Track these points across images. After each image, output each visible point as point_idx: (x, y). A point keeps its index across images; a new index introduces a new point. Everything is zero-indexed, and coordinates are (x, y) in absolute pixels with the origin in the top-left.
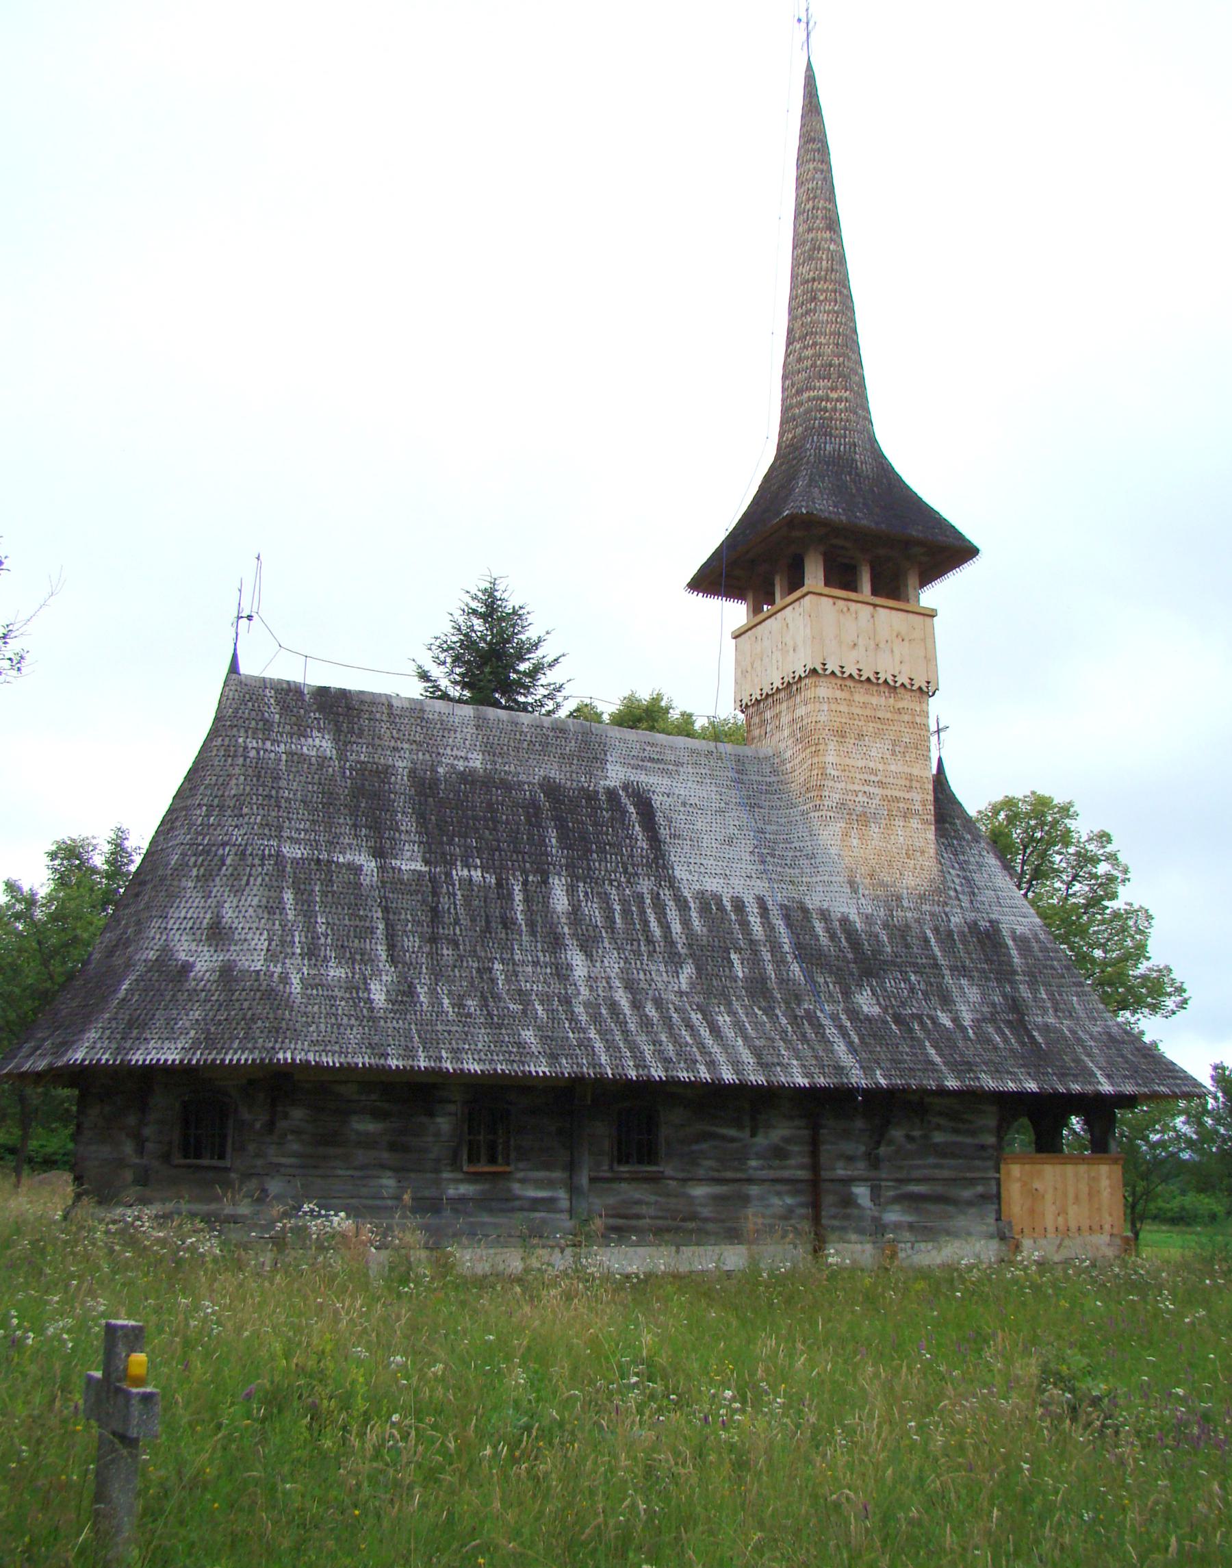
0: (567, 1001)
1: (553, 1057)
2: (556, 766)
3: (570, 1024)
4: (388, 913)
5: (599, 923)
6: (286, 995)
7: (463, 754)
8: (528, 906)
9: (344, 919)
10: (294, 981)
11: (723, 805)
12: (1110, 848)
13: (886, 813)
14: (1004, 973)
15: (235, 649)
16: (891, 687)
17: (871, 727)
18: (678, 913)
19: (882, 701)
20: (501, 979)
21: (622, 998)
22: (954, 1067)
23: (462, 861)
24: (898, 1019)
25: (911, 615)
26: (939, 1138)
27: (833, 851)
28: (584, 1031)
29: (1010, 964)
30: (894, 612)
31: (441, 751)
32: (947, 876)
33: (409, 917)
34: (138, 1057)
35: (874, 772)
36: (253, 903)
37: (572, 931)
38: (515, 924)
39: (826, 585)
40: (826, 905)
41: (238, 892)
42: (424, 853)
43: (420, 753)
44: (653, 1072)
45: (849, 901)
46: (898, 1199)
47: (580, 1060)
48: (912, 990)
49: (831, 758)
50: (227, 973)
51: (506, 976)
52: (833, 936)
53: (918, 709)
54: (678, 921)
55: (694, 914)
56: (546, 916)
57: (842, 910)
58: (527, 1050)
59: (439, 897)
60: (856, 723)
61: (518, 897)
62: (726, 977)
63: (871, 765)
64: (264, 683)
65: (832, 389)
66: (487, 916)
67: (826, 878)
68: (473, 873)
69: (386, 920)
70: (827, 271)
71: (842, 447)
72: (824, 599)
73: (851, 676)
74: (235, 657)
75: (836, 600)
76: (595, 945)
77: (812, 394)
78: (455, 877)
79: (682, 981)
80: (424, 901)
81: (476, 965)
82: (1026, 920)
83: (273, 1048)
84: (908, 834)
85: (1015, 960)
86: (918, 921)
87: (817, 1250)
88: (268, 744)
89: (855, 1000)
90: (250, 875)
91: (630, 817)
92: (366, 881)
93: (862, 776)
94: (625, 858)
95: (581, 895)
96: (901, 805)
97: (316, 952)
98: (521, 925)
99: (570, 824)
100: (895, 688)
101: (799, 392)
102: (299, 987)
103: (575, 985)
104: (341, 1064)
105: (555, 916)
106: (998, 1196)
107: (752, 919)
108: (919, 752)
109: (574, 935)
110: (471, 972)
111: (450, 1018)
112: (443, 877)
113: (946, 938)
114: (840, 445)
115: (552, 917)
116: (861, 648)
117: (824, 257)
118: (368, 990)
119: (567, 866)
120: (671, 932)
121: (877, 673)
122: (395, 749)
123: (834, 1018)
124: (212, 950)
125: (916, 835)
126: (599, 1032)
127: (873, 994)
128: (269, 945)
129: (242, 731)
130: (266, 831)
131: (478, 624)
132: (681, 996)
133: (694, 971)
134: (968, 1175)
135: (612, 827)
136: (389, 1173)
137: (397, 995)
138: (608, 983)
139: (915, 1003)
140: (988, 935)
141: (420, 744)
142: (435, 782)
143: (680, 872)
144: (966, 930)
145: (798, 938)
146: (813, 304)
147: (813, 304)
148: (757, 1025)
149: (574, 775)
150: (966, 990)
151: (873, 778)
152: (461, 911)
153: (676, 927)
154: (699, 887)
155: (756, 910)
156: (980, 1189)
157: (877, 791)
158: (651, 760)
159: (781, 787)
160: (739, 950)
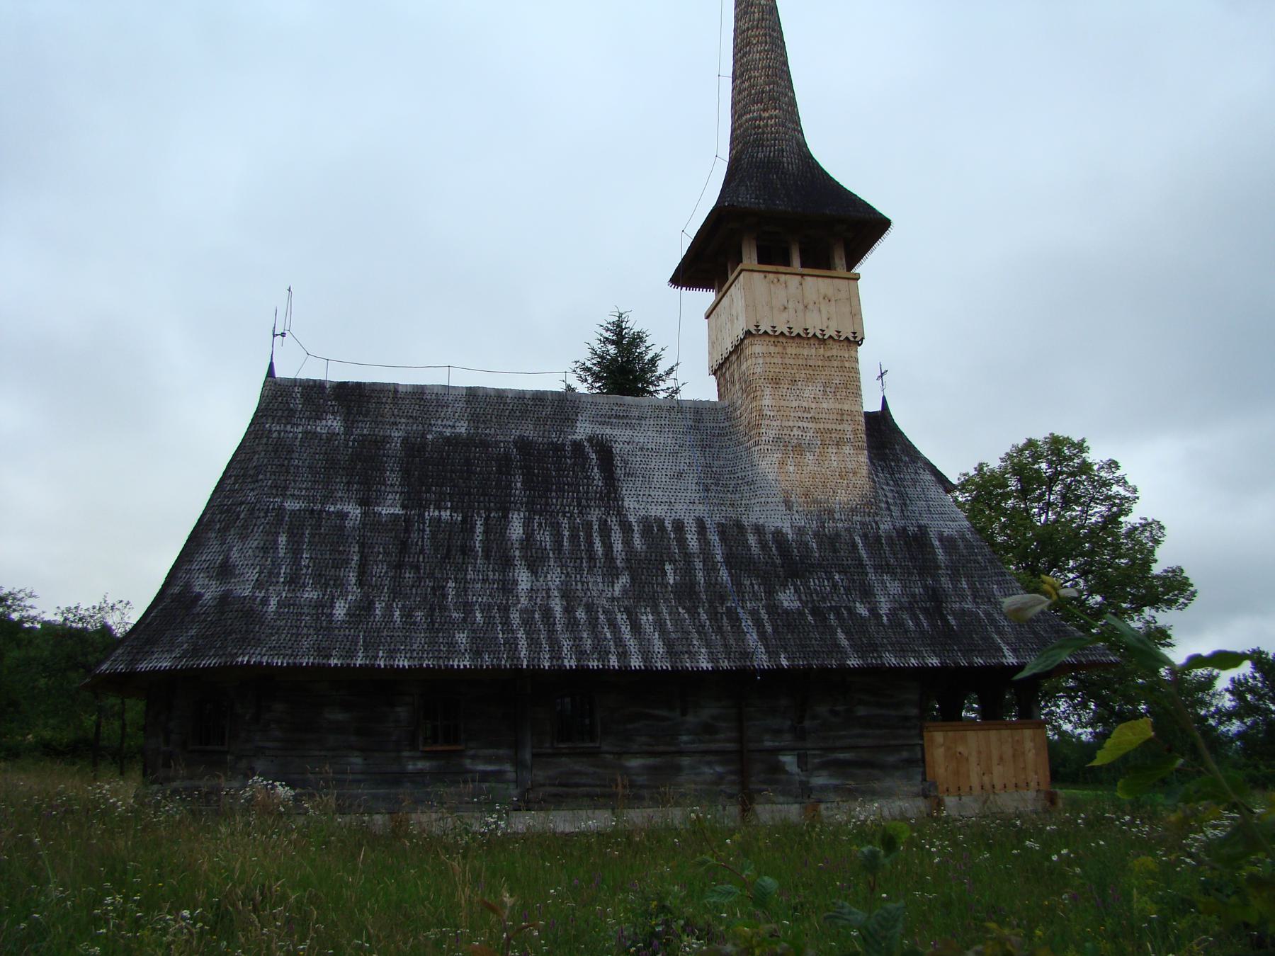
0: (505, 610)
1: (477, 653)
2: (531, 427)
3: (502, 627)
4: (364, 548)
5: (548, 547)
6: (262, 613)
7: (451, 424)
8: (487, 536)
9: (326, 554)
10: (272, 603)
11: (677, 447)
12: (1118, 473)
13: (819, 443)
14: (926, 566)
15: (272, 359)
16: (822, 340)
17: (803, 374)
18: (621, 535)
20: (451, 593)
21: (557, 606)
22: (860, 650)
23: (435, 505)
24: (814, 612)
26: (861, 711)
27: (771, 477)
28: (513, 631)
29: (935, 560)
30: (820, 279)
31: (433, 422)
32: (880, 492)
33: (381, 550)
34: (143, 666)
35: (806, 410)
36: (253, 546)
37: (522, 554)
38: (473, 551)
39: (759, 263)
40: (761, 521)
41: (243, 538)
42: (404, 500)
43: (415, 425)
44: (566, 663)
45: (783, 517)
46: (825, 766)
47: (501, 655)
48: (835, 586)
49: (767, 401)
50: (224, 600)
51: (457, 591)
52: (764, 546)
53: (846, 356)
54: (620, 542)
55: (636, 535)
56: (501, 543)
57: (776, 525)
58: (457, 648)
59: (410, 533)
60: (789, 371)
61: (479, 529)
62: (657, 584)
63: (805, 404)
64: (295, 382)
65: (765, 110)
66: (449, 546)
67: (763, 500)
68: (443, 513)
69: (362, 553)
70: (759, 20)
71: (772, 154)
72: (756, 274)
73: (782, 333)
74: (271, 365)
75: (767, 274)
76: (542, 564)
77: (748, 116)
78: (427, 517)
79: (616, 588)
80: (396, 537)
81: (431, 584)
82: (954, 523)
83: (236, 654)
84: (841, 459)
87: (746, 809)
88: (289, 427)
89: (776, 598)
90: (255, 525)
92: (349, 524)
93: (796, 414)
94: (581, 495)
95: (536, 525)
96: (833, 435)
97: (297, 580)
98: (478, 551)
99: (536, 471)
100: (825, 340)
101: (740, 117)
102: (275, 607)
103: (517, 596)
104: (288, 664)
105: (509, 543)
106: (923, 760)
107: (689, 537)
109: (522, 558)
110: (426, 590)
111: (396, 626)
112: (416, 517)
113: (873, 541)
114: (770, 152)
115: (506, 544)
116: (791, 311)
117: (756, 10)
118: (332, 607)
119: (527, 503)
120: (613, 551)
121: (807, 329)
122: (395, 424)
123: (754, 614)
124: (218, 583)
126: (527, 633)
127: (796, 591)
128: (259, 576)
129: (270, 419)
130: (274, 492)
131: (612, 349)
132: (613, 601)
133: (628, 581)
134: (892, 742)
135: (573, 471)
136: (356, 753)
137: (356, 610)
138: (547, 593)
139: (835, 598)
140: (915, 537)
141: (416, 418)
142: (424, 446)
143: (629, 503)
144: (895, 534)
145: (731, 549)
146: (748, 48)
147: (748, 48)
148: (677, 621)
149: (546, 433)
150: (888, 585)
151: (806, 415)
152: (427, 542)
153: (618, 546)
154: (644, 513)
155: (693, 529)
156: (905, 755)
157: (810, 425)
158: (617, 417)
159: (732, 430)
160: (673, 561)
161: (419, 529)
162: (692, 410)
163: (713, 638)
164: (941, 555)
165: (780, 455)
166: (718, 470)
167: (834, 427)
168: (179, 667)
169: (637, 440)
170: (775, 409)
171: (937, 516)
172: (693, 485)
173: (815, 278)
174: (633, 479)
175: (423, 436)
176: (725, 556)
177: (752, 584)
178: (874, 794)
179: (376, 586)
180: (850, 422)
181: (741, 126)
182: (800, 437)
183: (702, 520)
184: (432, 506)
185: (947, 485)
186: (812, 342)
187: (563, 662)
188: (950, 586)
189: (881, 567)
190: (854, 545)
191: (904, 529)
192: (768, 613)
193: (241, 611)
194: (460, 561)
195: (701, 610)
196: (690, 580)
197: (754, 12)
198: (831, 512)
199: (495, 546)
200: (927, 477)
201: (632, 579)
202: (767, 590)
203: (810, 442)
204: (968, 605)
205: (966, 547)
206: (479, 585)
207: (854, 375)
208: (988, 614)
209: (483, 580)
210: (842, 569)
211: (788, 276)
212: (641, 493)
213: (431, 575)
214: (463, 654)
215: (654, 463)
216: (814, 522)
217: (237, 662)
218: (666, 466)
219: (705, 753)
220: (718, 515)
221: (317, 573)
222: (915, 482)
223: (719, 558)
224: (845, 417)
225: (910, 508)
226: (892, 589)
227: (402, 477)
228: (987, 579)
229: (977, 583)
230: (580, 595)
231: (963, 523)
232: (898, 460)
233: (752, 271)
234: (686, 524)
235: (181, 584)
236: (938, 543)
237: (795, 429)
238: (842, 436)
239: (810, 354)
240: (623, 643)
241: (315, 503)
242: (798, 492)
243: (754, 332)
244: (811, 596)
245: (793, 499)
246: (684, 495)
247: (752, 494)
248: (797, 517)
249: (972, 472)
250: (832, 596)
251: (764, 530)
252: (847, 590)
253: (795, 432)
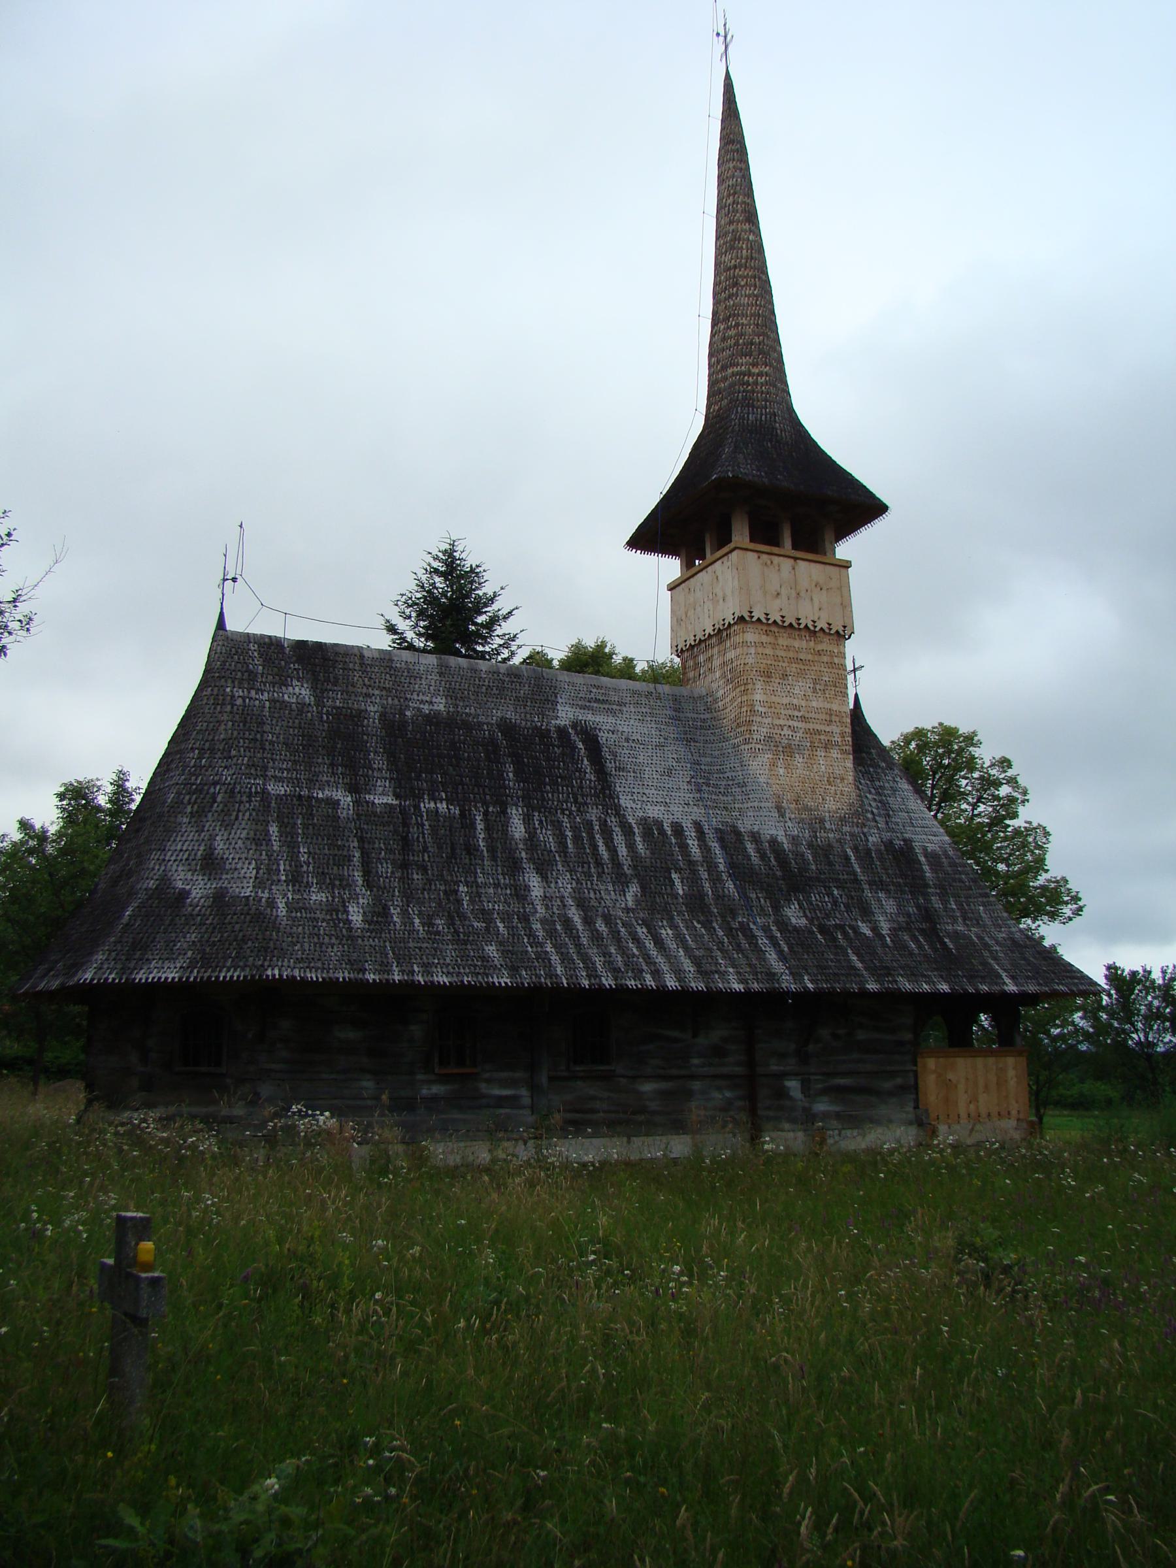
0: (525, 919)
1: (514, 970)
3: (529, 939)
4: (363, 842)
6: (273, 918)
7: (428, 699)
10: (280, 905)
12: (1010, 773)
13: (808, 744)
14: (917, 886)
15: (222, 608)
16: (812, 632)
19: (804, 644)
23: (429, 795)
24: (823, 930)
25: (828, 567)
26: (861, 1035)
27: (762, 779)
29: (923, 878)
30: (813, 565)
31: (409, 696)
34: (141, 976)
35: (797, 708)
36: (242, 836)
37: (529, 856)
38: (478, 850)
40: (756, 828)
41: (228, 826)
42: (395, 788)
43: (390, 699)
46: (826, 1091)
48: (835, 903)
49: (758, 696)
50: (220, 899)
51: (470, 897)
52: (763, 856)
53: (836, 651)
54: (624, 845)
56: (506, 843)
57: (771, 832)
59: (409, 828)
62: (667, 894)
63: (795, 701)
64: (248, 638)
65: (754, 365)
66: (452, 844)
67: (756, 804)
69: (362, 848)
70: (747, 258)
71: (763, 417)
72: (750, 554)
73: (775, 622)
74: (222, 615)
77: (735, 369)
78: (423, 809)
79: (629, 898)
81: (443, 888)
83: (262, 966)
85: (927, 874)
86: (839, 841)
87: (754, 1138)
88: (253, 692)
90: (239, 811)
91: (579, 752)
92: (343, 814)
93: (787, 712)
95: (537, 823)
96: (822, 737)
98: (483, 851)
100: (815, 632)
103: (533, 904)
105: (513, 843)
106: (916, 1087)
109: (529, 860)
111: (421, 936)
112: (412, 809)
113: (865, 855)
114: (762, 414)
117: (744, 246)
121: (799, 619)
122: (367, 695)
123: (766, 929)
127: (800, 908)
128: (257, 873)
129: (230, 681)
130: (253, 771)
132: (628, 913)
137: (373, 916)
141: (389, 690)
142: (403, 724)
143: (625, 801)
144: (883, 848)
148: (696, 937)
149: (528, 716)
151: (796, 713)
152: (429, 839)
153: (623, 851)
154: (642, 814)
156: (899, 1081)
157: (800, 725)
158: (597, 701)
159: (714, 723)
160: (678, 870)
161: (417, 823)
163: (735, 956)
168: (192, 979)
175: (402, 714)
177: (758, 898)
178: (876, 1122)
179: (385, 888)
181: (725, 379)
184: (426, 797)
187: (600, 979)
190: (847, 858)
191: (891, 842)
193: (248, 914)
194: (467, 861)
195: (715, 924)
196: (698, 891)
198: (822, 821)
199: (499, 845)
201: (643, 888)
206: (491, 890)
208: (980, 938)
209: (495, 884)
211: (782, 558)
213: (441, 877)
214: (500, 970)
217: (267, 976)
219: (715, 1077)
221: (320, 870)
222: (894, 790)
227: (388, 761)
230: (595, 904)
231: (942, 838)
232: (877, 766)
234: (685, 829)
235: (155, 877)
237: (785, 728)
240: (652, 960)
241: (301, 789)
243: (748, 619)
248: (790, 825)
252: (847, 906)
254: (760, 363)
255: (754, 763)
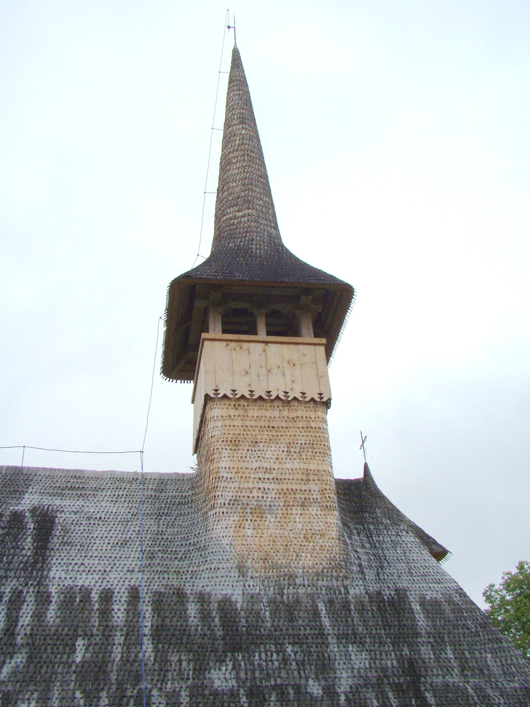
11: (130, 516)
13: (282, 504)
19: (277, 413)
25: (301, 347)
27: (225, 541)
29: (414, 626)
30: (285, 347)
35: (267, 470)
40: (208, 589)
45: (235, 584)
48: (285, 661)
49: (225, 463)
53: (313, 416)
54: (30, 615)
55: (53, 607)
57: (224, 592)
65: (239, 211)
72: (217, 343)
75: (229, 343)
77: (225, 217)
82: (439, 586)
84: (307, 520)
85: (420, 623)
86: (310, 596)
89: (207, 676)
91: (27, 531)
107: (116, 607)
108: (315, 450)
114: (241, 242)
125: (315, 521)
127: (234, 668)
133: (24, 660)
139: (283, 674)
140: (391, 602)
144: (367, 599)
146: (228, 167)
150: (353, 657)
151: (267, 476)
157: (271, 486)
162: (156, 482)
164: (421, 620)
165: (236, 518)
166: (170, 537)
167: (298, 487)
169: (87, 509)
170: (234, 471)
171: (419, 578)
172: (137, 553)
173: (279, 345)
174: (68, 548)
176: (154, 628)
180: (317, 482)
182: (260, 498)
183: (137, 589)
185: (434, 546)
186: (276, 404)
188: (432, 656)
189: (346, 636)
190: (316, 613)
191: (379, 593)
192: (191, 696)
196: (103, 657)
197: (236, 140)
198: (292, 577)
200: (411, 539)
202: (197, 667)
203: (272, 504)
204: (454, 679)
205: (453, 611)
207: (321, 435)
208: (478, 689)
210: (297, 640)
212: (73, 562)
215: (98, 532)
216: (272, 589)
218: (111, 534)
220: (157, 584)
222: (395, 544)
223: (147, 631)
224: (311, 477)
225: (387, 571)
226: (357, 662)
228: (478, 647)
229: (466, 653)
233: (214, 340)
236: (418, 607)
237: (255, 491)
238: (307, 497)
239: (273, 416)
242: (255, 557)
244: (253, 672)
245: (249, 564)
246: (123, 563)
247: (202, 560)
248: (251, 583)
249: (515, 571)
250: (280, 673)
251: (209, 598)
252: (301, 664)
253: (255, 493)
254: (244, 208)
255: (219, 526)
